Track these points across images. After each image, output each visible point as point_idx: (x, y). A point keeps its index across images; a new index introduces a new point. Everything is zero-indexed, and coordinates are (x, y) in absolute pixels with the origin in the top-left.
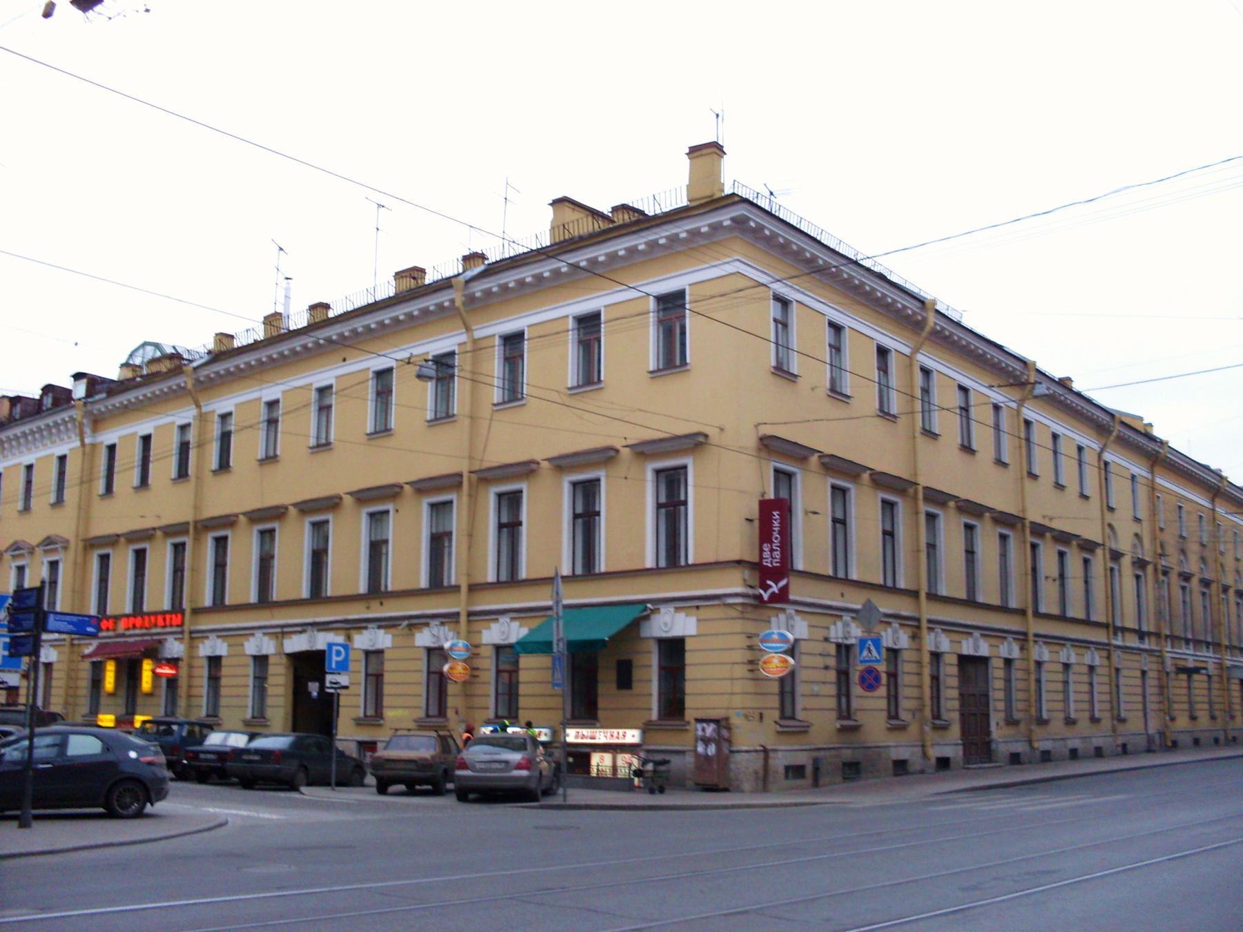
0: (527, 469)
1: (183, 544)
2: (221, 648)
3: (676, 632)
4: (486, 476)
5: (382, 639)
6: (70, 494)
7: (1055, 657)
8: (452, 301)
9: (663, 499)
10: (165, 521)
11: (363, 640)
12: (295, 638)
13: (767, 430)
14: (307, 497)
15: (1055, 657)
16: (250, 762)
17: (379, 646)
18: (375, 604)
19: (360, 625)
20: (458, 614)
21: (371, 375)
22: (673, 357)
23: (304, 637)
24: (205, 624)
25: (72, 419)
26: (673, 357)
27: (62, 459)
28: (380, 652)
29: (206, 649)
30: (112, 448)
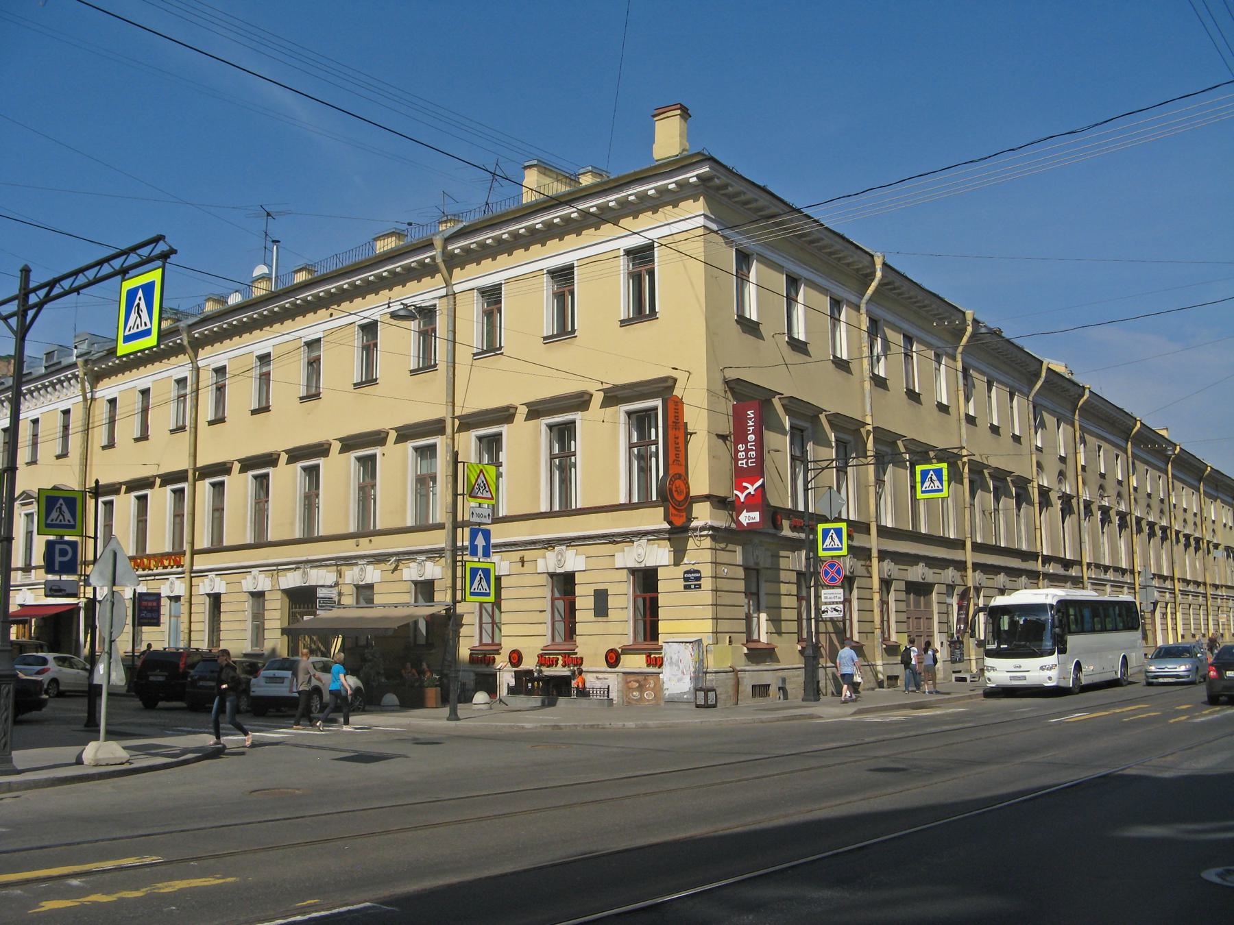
0: (505, 415)
1: (182, 490)
2: (219, 585)
3: (650, 562)
4: (468, 422)
5: (373, 574)
6: (75, 441)
7: (235, 588)
8: (433, 258)
9: (635, 439)
10: (163, 470)
11: (351, 575)
12: (290, 574)
13: (732, 375)
14: (249, 454)
15: (235, 588)
16: (206, 688)
17: (368, 580)
18: (364, 541)
19: (350, 561)
20: (443, 549)
21: (622, 253)
22: (643, 309)
23: (298, 573)
24: (201, 563)
25: (76, 377)
26: (643, 309)
27: (66, 412)
28: (370, 587)
29: (204, 586)
30: (113, 402)
